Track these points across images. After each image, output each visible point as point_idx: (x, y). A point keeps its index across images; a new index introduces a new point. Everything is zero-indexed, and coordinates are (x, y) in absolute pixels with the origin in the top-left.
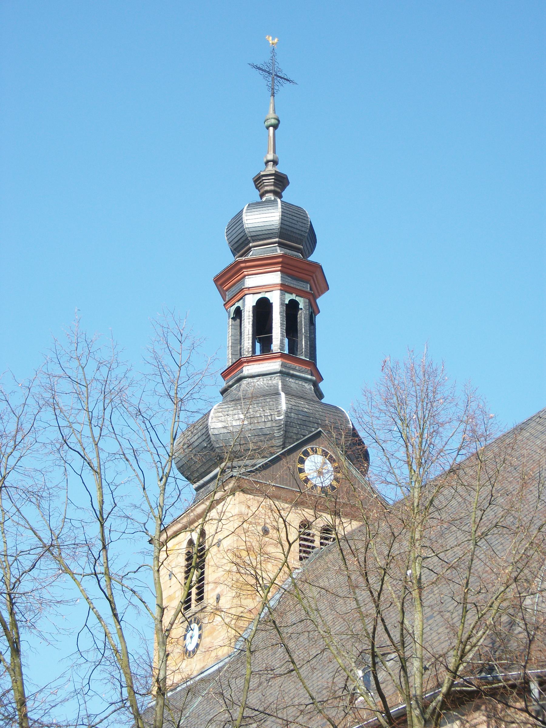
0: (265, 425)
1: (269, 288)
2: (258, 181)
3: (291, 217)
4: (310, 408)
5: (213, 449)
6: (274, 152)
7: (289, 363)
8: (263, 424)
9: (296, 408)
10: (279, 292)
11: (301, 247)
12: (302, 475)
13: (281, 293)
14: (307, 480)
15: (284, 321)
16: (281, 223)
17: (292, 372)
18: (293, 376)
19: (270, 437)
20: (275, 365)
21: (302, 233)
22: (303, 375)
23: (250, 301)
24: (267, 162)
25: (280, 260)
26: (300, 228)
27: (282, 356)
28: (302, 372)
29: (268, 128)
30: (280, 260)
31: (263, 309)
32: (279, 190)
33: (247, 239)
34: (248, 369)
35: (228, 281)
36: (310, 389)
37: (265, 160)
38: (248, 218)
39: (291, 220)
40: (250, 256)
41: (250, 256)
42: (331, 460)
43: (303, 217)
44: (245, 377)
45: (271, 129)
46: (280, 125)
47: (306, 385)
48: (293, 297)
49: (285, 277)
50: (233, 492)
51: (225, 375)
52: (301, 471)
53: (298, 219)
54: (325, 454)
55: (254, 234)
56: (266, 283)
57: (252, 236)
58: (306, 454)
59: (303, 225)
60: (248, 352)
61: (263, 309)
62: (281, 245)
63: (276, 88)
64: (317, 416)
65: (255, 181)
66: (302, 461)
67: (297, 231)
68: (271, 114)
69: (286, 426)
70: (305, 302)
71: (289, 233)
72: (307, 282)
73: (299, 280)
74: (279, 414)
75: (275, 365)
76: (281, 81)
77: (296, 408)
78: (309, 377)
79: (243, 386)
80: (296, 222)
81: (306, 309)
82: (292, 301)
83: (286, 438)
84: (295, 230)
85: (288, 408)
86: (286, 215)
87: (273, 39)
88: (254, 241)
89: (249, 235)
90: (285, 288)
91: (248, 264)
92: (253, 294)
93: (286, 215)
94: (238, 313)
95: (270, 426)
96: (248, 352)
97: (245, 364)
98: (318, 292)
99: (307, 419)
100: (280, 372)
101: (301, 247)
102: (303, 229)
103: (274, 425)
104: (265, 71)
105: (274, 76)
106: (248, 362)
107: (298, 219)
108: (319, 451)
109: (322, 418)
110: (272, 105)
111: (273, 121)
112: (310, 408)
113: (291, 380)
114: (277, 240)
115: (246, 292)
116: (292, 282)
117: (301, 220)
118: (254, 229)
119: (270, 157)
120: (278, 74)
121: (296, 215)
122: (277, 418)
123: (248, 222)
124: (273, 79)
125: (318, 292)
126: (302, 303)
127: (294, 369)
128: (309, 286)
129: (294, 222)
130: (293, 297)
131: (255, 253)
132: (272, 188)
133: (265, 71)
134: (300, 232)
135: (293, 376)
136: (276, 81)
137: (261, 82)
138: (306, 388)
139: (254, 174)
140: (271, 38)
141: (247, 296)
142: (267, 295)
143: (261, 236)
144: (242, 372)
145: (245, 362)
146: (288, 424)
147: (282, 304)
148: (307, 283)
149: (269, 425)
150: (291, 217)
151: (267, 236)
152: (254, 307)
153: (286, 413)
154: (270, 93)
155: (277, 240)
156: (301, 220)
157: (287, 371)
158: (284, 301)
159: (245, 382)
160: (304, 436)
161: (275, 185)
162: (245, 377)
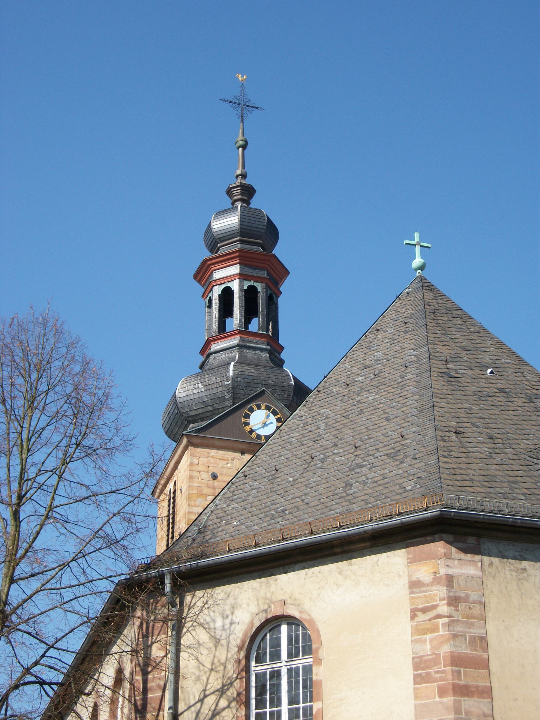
0: (218, 390)
1: (230, 278)
2: (229, 192)
3: (249, 218)
4: (256, 372)
5: (181, 414)
6: (243, 167)
7: (247, 337)
8: (216, 389)
9: (243, 373)
10: (238, 280)
11: (261, 241)
12: (247, 428)
13: (240, 281)
14: (252, 431)
15: (242, 304)
16: (241, 224)
17: (248, 344)
18: (249, 348)
19: (222, 399)
20: (235, 341)
21: (261, 230)
22: (259, 346)
23: (217, 291)
24: (237, 176)
25: (237, 254)
26: (258, 226)
27: (240, 332)
28: (259, 344)
29: (238, 148)
30: (237, 254)
31: (227, 294)
32: (246, 198)
33: (216, 241)
34: (215, 347)
35: (203, 274)
36: (266, 357)
37: (235, 175)
38: (215, 223)
39: (249, 221)
40: (219, 253)
41: (219, 253)
42: (275, 413)
43: (260, 217)
44: (212, 353)
45: (241, 149)
46: (248, 146)
47: (262, 354)
48: (252, 283)
49: (244, 267)
50: (186, 448)
51: (202, 352)
52: (247, 424)
53: (256, 219)
54: (268, 408)
55: (221, 236)
56: (229, 274)
57: (219, 238)
58: (252, 410)
59: (261, 223)
60: (215, 332)
61: (227, 294)
62: (241, 242)
63: (245, 115)
64: (262, 377)
65: (227, 194)
66: (247, 416)
67: (256, 229)
68: (240, 137)
69: (233, 388)
70: (262, 286)
71: (249, 232)
72: (263, 269)
73: (255, 269)
74: (227, 380)
75: (235, 341)
76: (250, 109)
77: (243, 373)
78: (264, 347)
79: (210, 360)
80: (254, 222)
81: (263, 292)
82: (250, 287)
83: (234, 399)
84: (253, 229)
85: (234, 374)
86: (244, 217)
87: (242, 76)
88: (222, 242)
89: (217, 237)
90: (242, 277)
91: (214, 261)
92: (219, 285)
93: (244, 217)
94: (210, 301)
95: (221, 390)
96: (215, 332)
97: (212, 343)
98: (279, 277)
99: (252, 381)
100: (238, 345)
101: (261, 241)
102: (261, 227)
103: (224, 389)
104: (235, 103)
105: (243, 107)
106: (215, 340)
107: (256, 219)
108: (263, 406)
109: (266, 379)
110: (241, 130)
111: (241, 143)
112: (256, 372)
113: (248, 351)
114: (238, 238)
115: (214, 284)
116: (250, 271)
117: (258, 220)
118: (220, 232)
119: (239, 172)
120: (247, 104)
121: (253, 216)
122: (226, 383)
123: (216, 227)
124: (243, 108)
125: (279, 277)
126: (260, 287)
127: (252, 342)
128: (266, 272)
129: (252, 222)
130: (252, 283)
131: (223, 251)
132: (240, 197)
133: (235, 103)
134: (258, 230)
135: (249, 348)
136: (245, 110)
137: (232, 113)
138: (262, 356)
139: (226, 188)
140: (240, 76)
141: (215, 288)
142: (229, 285)
143: (226, 236)
144: (210, 349)
145: (212, 341)
146: (235, 388)
147: (241, 290)
148: (265, 270)
149: (220, 389)
150: (249, 218)
151: (231, 236)
152: (219, 295)
153: (233, 378)
154: (240, 121)
155: (238, 238)
156: (258, 220)
157: (244, 344)
158: (243, 287)
159: (212, 357)
160: (250, 395)
161: (242, 194)
162: (212, 353)
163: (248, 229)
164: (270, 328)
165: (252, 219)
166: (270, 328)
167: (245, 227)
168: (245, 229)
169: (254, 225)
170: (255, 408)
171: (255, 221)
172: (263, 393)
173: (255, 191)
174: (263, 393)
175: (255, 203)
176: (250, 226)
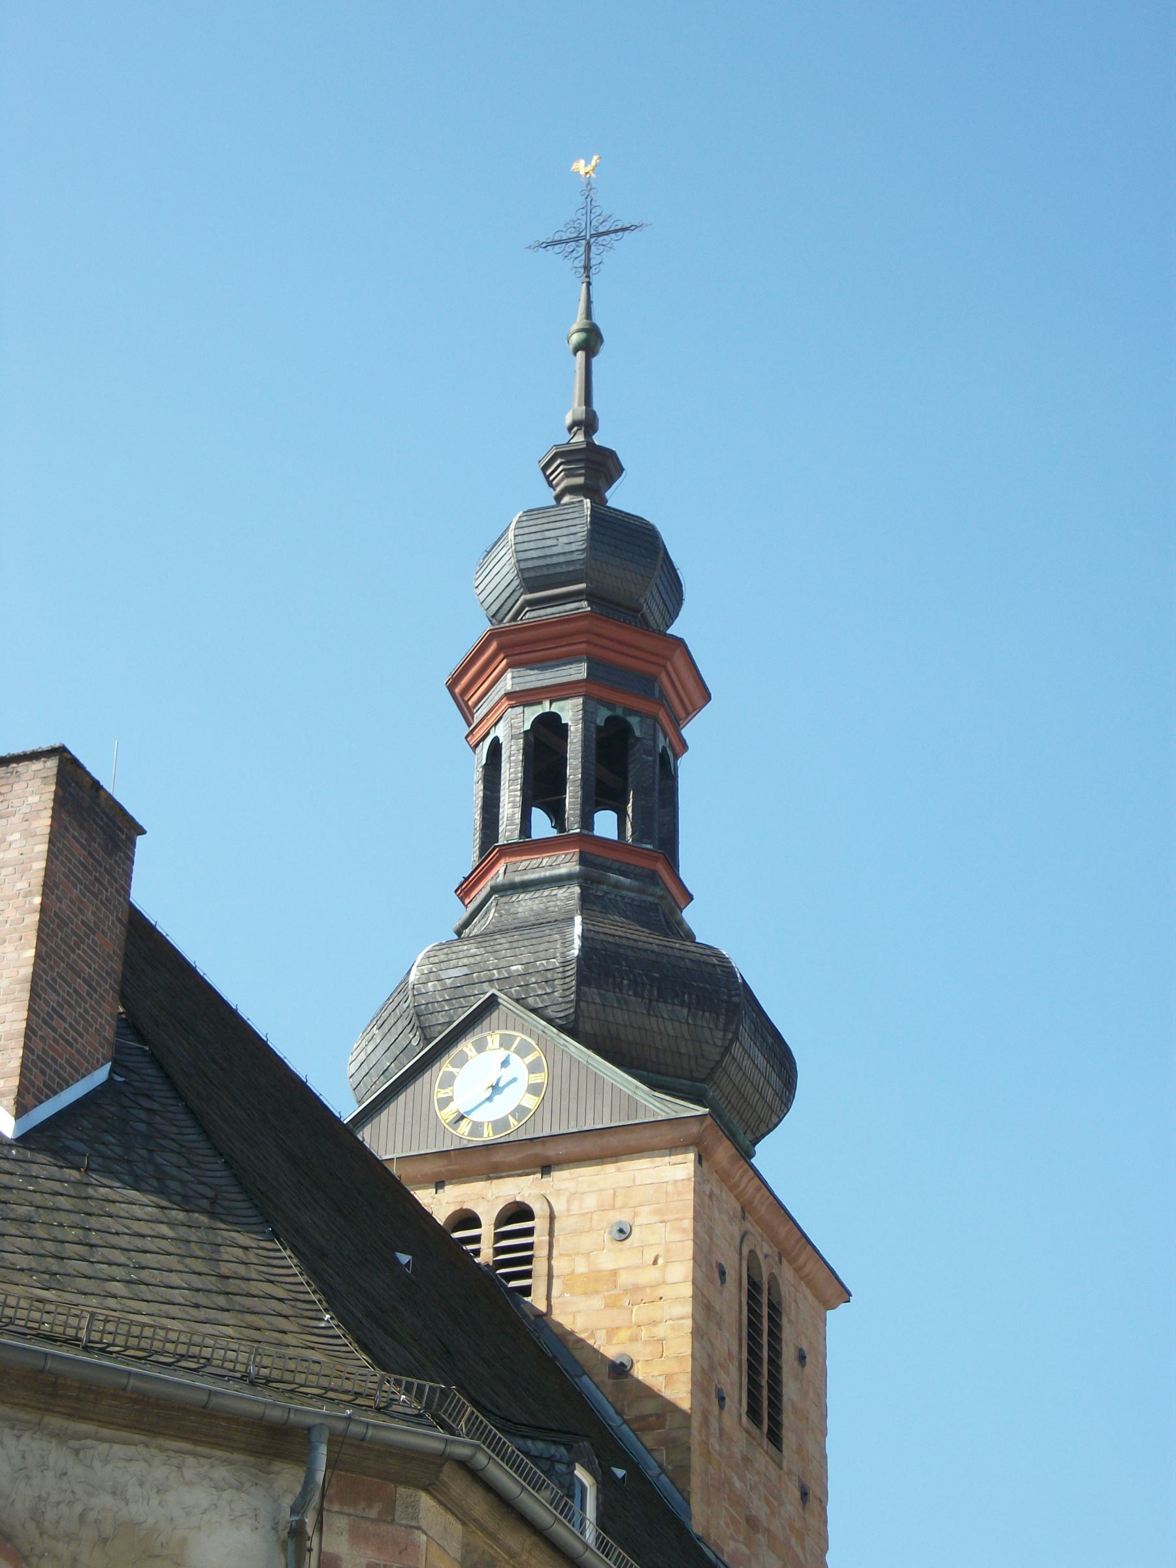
25: (494, 646)
26: (568, 549)
30: (494, 646)
71: (545, 572)
80: (553, 542)
81: (576, 722)
84: (555, 560)
109: (503, 963)
163: (540, 567)
164: (630, 811)
165: (547, 534)
166: (630, 811)
167: (530, 564)
168: (534, 568)
169: (555, 550)
170: (530, 1058)
171: (557, 538)
172: (491, 1004)
173: (621, 470)
174: (491, 1004)
175: (619, 497)
176: (545, 557)
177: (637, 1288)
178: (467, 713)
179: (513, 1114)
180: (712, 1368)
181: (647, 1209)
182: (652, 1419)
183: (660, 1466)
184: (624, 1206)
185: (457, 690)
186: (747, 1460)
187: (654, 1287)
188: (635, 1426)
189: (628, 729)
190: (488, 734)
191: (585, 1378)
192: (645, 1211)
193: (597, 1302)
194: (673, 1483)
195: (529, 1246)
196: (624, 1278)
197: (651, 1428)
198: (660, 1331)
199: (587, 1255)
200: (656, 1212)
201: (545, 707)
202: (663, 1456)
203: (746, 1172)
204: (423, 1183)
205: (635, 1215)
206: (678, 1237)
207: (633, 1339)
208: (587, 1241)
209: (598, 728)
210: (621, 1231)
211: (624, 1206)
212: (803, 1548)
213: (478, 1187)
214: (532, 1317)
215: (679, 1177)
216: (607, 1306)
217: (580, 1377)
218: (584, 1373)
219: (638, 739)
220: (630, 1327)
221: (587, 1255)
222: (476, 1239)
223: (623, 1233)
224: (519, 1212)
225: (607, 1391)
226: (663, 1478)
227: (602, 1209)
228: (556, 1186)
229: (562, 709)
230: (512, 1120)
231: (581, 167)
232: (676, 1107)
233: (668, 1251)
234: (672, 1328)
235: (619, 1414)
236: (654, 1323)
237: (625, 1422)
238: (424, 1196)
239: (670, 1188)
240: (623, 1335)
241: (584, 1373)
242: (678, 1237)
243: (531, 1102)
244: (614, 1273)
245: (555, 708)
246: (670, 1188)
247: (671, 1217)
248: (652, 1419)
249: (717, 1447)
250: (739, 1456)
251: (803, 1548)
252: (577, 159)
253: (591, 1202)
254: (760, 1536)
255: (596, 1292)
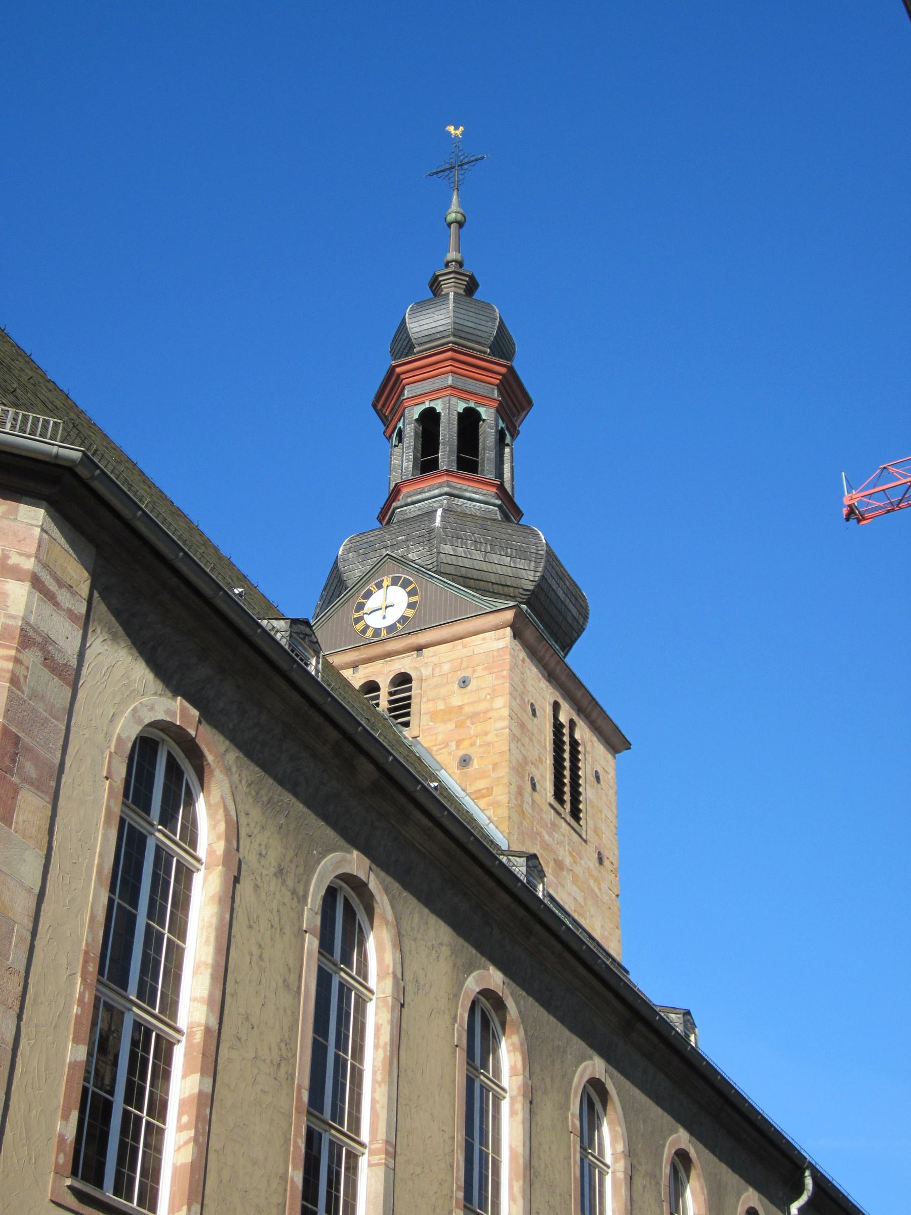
177: (476, 714)
178: (385, 420)
179: (398, 621)
180: (526, 763)
181: (481, 667)
182: (484, 791)
183: (489, 818)
184: (467, 667)
185: (379, 407)
186: (554, 825)
187: (486, 712)
188: (473, 797)
189: (478, 415)
190: (395, 427)
191: (443, 771)
192: (479, 669)
193: (451, 726)
194: (497, 828)
195: (409, 698)
196: (468, 710)
197: (483, 796)
198: (489, 738)
199: (444, 699)
200: (485, 669)
201: (427, 405)
202: (490, 812)
203: (547, 650)
204: (346, 666)
205: (474, 671)
206: (500, 682)
207: (473, 744)
208: (443, 691)
209: (459, 413)
210: (464, 682)
211: (467, 667)
212: (600, 889)
213: (378, 666)
214: (410, 739)
215: (501, 647)
216: (456, 727)
217: (439, 771)
218: (442, 768)
219: (484, 420)
220: (471, 738)
221: (444, 699)
222: (378, 697)
223: (464, 683)
224: (403, 679)
225: (455, 777)
226: (491, 825)
227: (454, 671)
228: (426, 660)
229: (437, 405)
230: (398, 625)
231: (451, 129)
232: (497, 604)
233: (494, 690)
234: (497, 735)
235: (463, 790)
236: (486, 734)
237: (467, 795)
238: (347, 673)
239: (495, 654)
240: (466, 743)
241: (442, 768)
242: (500, 682)
243: (410, 613)
244: (461, 707)
245: (432, 405)
246: (495, 654)
247: (495, 670)
248: (484, 791)
249: (530, 811)
250: (548, 822)
251: (600, 889)
252: (450, 124)
253: (446, 668)
254: (565, 873)
255: (450, 720)
